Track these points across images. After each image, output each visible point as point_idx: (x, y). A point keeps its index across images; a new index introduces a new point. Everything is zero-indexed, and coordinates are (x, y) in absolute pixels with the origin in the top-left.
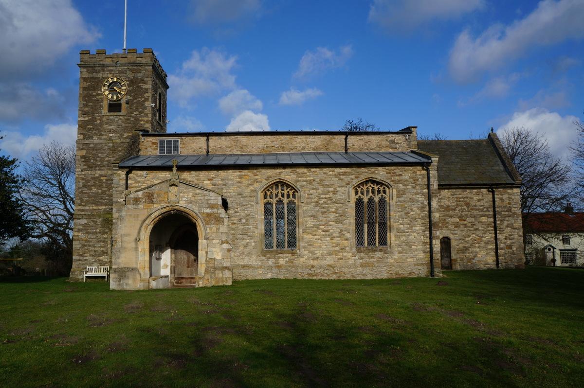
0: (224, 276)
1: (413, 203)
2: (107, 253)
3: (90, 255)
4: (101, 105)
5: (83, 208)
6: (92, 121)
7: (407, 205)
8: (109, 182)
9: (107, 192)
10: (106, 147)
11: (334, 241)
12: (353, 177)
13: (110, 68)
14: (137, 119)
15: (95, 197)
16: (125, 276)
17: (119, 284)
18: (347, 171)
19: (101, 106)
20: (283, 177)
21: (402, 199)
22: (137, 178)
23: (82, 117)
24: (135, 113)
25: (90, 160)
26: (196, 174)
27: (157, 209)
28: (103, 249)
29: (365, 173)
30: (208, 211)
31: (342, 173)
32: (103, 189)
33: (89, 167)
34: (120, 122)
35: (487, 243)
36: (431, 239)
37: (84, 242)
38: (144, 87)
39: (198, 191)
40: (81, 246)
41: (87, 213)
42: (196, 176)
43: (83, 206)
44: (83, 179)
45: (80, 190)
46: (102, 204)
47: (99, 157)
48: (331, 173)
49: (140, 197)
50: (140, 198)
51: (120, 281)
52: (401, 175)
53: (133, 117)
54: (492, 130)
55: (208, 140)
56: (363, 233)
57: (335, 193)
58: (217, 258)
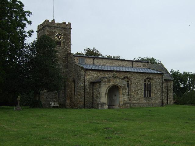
12: (144, 76)
14: (66, 49)
20: (127, 75)
21: (156, 84)
27: (112, 84)
30: (123, 86)
36: (162, 96)
54: (161, 62)
55: (94, 60)
57: (140, 81)
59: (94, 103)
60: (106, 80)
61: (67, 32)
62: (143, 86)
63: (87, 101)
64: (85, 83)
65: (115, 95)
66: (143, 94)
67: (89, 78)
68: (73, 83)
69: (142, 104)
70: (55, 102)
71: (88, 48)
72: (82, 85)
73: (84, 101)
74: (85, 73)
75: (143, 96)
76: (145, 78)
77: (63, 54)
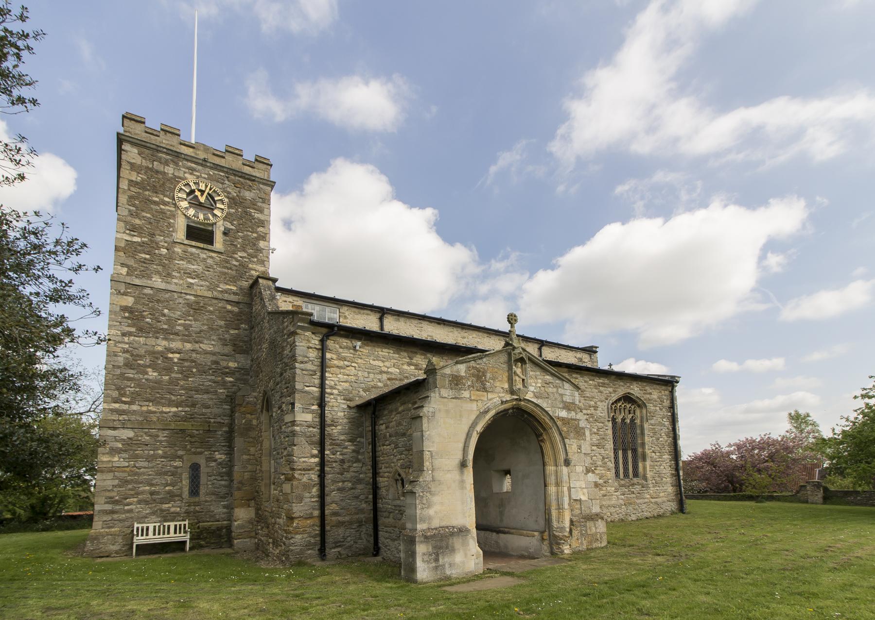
0: (598, 530)
1: (662, 428)
2: (180, 496)
3: (139, 502)
4: (169, 223)
5: (125, 407)
6: (151, 247)
8: (186, 364)
9: (182, 383)
10: (181, 300)
12: (611, 390)
13: (189, 164)
15: (152, 388)
16: (447, 548)
17: (436, 568)
22: (341, 350)
23: (124, 232)
24: (240, 254)
25: (144, 317)
28: (171, 488)
29: (622, 389)
30: (563, 414)
32: (173, 375)
33: (140, 329)
34: (210, 261)
37: (126, 475)
38: (256, 215)
39: (548, 377)
40: (116, 482)
41: (133, 418)
43: (125, 403)
44: (127, 351)
45: (118, 372)
46: (170, 404)
47: (164, 315)
48: (591, 382)
49: (463, 374)
50: (462, 377)
51: (437, 560)
52: (650, 394)
53: (237, 260)
56: (627, 462)
57: (596, 408)
58: (584, 498)
59: (382, 521)
61: (248, 195)
62: (610, 432)
63: (335, 514)
64: (322, 404)
66: (612, 465)
67: (353, 378)
69: (612, 510)
72: (309, 417)
73: (316, 513)
74: (323, 349)
75: (611, 474)
76: (615, 397)
77: (223, 287)
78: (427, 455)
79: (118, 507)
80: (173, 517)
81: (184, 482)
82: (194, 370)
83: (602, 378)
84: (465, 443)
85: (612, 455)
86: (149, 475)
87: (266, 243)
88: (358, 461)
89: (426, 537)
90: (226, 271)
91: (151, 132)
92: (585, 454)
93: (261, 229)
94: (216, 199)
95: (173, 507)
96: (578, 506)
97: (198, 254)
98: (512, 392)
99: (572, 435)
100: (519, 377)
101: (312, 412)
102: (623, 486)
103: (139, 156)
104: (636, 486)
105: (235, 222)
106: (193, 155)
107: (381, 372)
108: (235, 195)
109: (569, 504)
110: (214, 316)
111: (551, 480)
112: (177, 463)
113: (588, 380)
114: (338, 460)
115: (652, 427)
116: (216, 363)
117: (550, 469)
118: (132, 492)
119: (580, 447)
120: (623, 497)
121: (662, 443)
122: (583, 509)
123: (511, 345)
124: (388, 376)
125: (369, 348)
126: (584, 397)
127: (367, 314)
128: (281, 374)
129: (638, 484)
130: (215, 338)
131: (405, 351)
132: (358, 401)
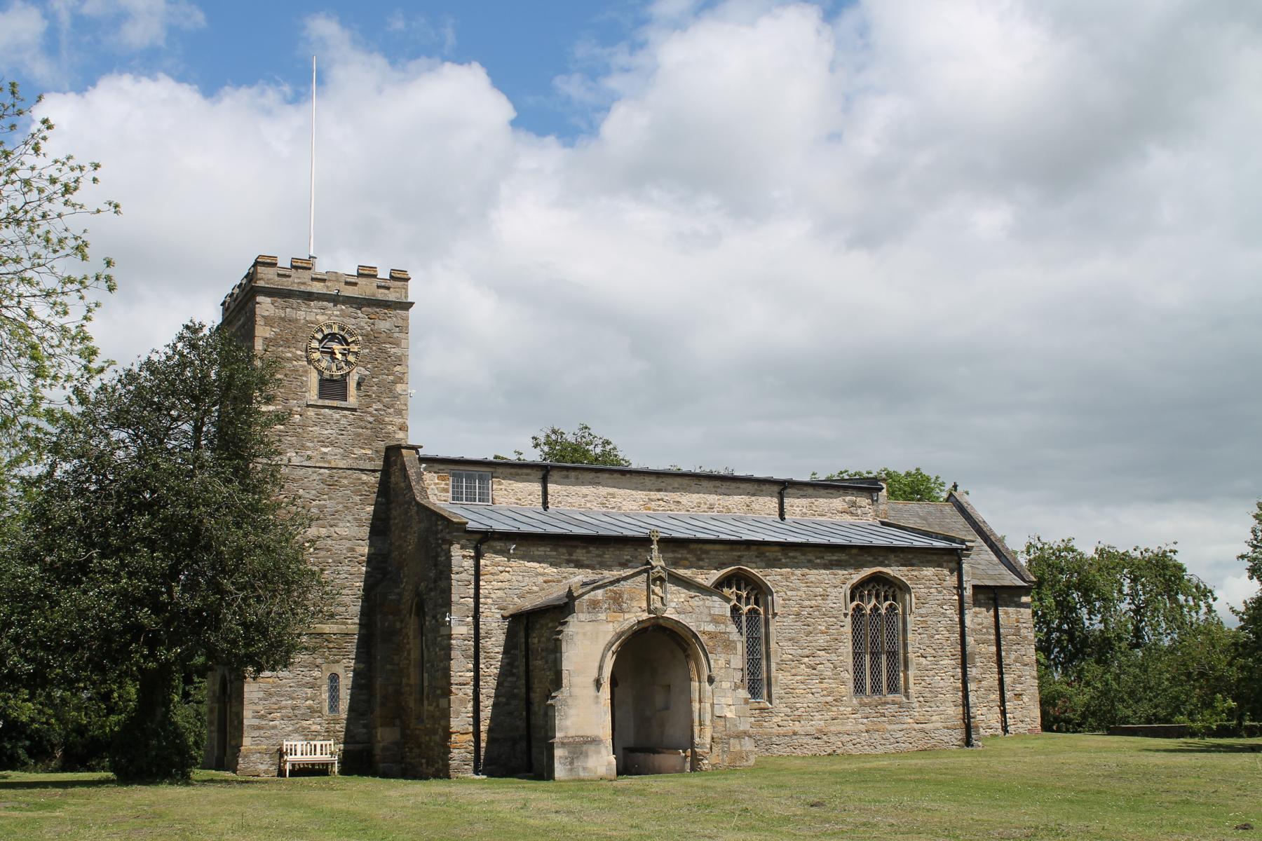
1: (940, 619)
7: (931, 620)
11: (824, 686)
17: (571, 770)
18: (843, 558)
19: (303, 385)
21: (923, 611)
26: (597, 552)
27: (636, 614)
30: (710, 628)
31: (836, 560)
34: (343, 421)
35: (988, 690)
40: (261, 695)
42: (598, 556)
48: (818, 561)
51: (572, 763)
57: (824, 597)
58: (729, 715)
60: (600, 592)
61: (383, 325)
65: (668, 687)
66: (849, 676)
68: (412, 621)
69: (846, 738)
70: (308, 735)
71: (554, 432)
74: (477, 558)
78: (565, 674)
79: (264, 722)
80: (315, 735)
81: (323, 696)
82: (330, 561)
83: (837, 554)
84: (601, 661)
85: (850, 661)
86: (290, 687)
87: (403, 386)
88: (512, 674)
89: (562, 743)
90: (360, 430)
91: (284, 273)
92: (734, 669)
93: (398, 368)
94: (350, 340)
95: (314, 725)
96: (723, 723)
97: (331, 415)
98: (650, 612)
99: (719, 649)
100: (658, 595)
101: (467, 624)
102: (865, 705)
103: (272, 306)
104: (889, 706)
105: (369, 366)
106: (325, 291)
107: (538, 574)
108: (369, 329)
109: (712, 721)
110: (349, 492)
111: (696, 696)
112: (316, 673)
113: (813, 558)
114: (492, 674)
115: (922, 619)
116: (352, 550)
117: (695, 685)
118: (276, 707)
119: (728, 662)
120: (865, 720)
121: (938, 641)
122: (728, 726)
123: (651, 564)
124: (545, 579)
125: (524, 549)
126: (807, 583)
127: (527, 475)
128: (435, 581)
129: (894, 703)
130: (350, 518)
131: (564, 546)
132: (512, 609)
